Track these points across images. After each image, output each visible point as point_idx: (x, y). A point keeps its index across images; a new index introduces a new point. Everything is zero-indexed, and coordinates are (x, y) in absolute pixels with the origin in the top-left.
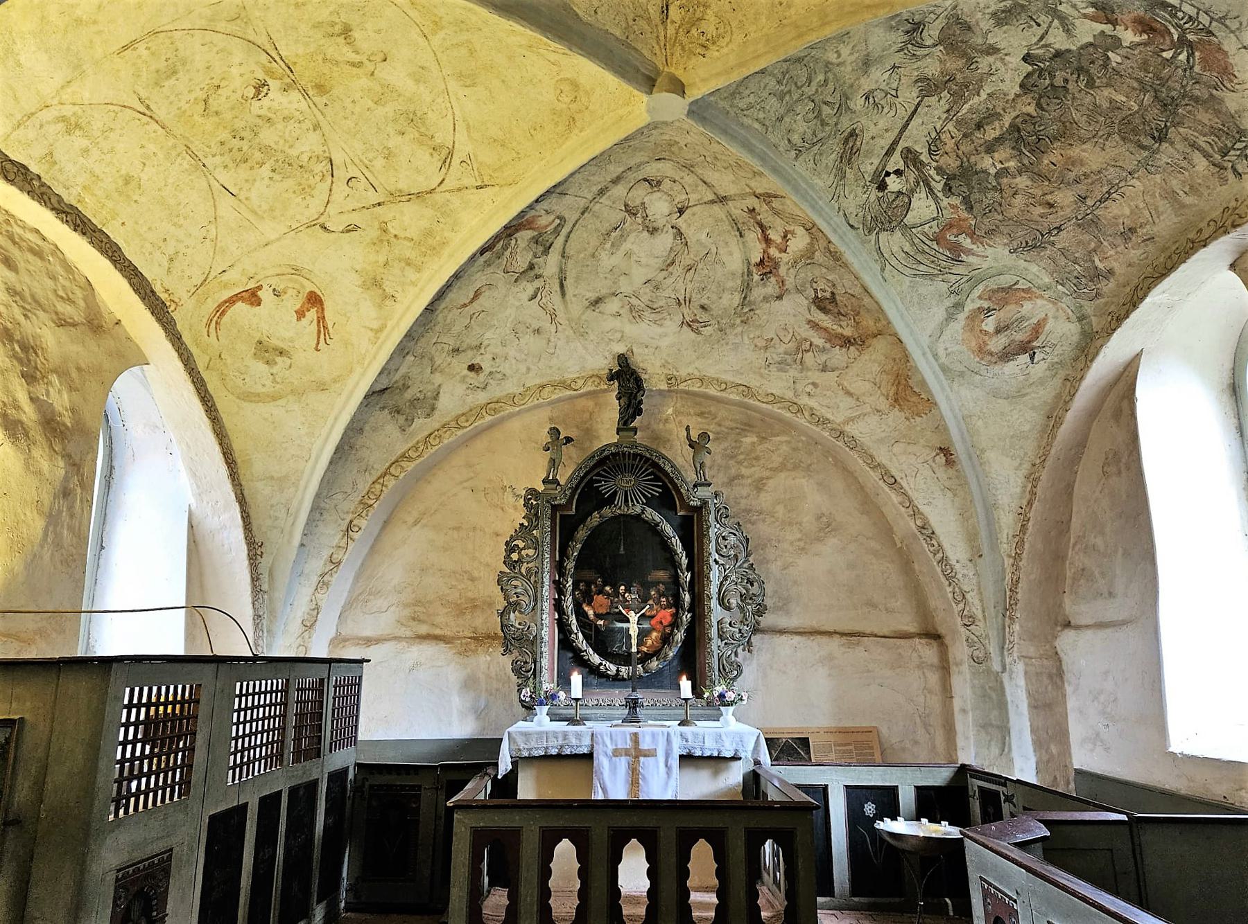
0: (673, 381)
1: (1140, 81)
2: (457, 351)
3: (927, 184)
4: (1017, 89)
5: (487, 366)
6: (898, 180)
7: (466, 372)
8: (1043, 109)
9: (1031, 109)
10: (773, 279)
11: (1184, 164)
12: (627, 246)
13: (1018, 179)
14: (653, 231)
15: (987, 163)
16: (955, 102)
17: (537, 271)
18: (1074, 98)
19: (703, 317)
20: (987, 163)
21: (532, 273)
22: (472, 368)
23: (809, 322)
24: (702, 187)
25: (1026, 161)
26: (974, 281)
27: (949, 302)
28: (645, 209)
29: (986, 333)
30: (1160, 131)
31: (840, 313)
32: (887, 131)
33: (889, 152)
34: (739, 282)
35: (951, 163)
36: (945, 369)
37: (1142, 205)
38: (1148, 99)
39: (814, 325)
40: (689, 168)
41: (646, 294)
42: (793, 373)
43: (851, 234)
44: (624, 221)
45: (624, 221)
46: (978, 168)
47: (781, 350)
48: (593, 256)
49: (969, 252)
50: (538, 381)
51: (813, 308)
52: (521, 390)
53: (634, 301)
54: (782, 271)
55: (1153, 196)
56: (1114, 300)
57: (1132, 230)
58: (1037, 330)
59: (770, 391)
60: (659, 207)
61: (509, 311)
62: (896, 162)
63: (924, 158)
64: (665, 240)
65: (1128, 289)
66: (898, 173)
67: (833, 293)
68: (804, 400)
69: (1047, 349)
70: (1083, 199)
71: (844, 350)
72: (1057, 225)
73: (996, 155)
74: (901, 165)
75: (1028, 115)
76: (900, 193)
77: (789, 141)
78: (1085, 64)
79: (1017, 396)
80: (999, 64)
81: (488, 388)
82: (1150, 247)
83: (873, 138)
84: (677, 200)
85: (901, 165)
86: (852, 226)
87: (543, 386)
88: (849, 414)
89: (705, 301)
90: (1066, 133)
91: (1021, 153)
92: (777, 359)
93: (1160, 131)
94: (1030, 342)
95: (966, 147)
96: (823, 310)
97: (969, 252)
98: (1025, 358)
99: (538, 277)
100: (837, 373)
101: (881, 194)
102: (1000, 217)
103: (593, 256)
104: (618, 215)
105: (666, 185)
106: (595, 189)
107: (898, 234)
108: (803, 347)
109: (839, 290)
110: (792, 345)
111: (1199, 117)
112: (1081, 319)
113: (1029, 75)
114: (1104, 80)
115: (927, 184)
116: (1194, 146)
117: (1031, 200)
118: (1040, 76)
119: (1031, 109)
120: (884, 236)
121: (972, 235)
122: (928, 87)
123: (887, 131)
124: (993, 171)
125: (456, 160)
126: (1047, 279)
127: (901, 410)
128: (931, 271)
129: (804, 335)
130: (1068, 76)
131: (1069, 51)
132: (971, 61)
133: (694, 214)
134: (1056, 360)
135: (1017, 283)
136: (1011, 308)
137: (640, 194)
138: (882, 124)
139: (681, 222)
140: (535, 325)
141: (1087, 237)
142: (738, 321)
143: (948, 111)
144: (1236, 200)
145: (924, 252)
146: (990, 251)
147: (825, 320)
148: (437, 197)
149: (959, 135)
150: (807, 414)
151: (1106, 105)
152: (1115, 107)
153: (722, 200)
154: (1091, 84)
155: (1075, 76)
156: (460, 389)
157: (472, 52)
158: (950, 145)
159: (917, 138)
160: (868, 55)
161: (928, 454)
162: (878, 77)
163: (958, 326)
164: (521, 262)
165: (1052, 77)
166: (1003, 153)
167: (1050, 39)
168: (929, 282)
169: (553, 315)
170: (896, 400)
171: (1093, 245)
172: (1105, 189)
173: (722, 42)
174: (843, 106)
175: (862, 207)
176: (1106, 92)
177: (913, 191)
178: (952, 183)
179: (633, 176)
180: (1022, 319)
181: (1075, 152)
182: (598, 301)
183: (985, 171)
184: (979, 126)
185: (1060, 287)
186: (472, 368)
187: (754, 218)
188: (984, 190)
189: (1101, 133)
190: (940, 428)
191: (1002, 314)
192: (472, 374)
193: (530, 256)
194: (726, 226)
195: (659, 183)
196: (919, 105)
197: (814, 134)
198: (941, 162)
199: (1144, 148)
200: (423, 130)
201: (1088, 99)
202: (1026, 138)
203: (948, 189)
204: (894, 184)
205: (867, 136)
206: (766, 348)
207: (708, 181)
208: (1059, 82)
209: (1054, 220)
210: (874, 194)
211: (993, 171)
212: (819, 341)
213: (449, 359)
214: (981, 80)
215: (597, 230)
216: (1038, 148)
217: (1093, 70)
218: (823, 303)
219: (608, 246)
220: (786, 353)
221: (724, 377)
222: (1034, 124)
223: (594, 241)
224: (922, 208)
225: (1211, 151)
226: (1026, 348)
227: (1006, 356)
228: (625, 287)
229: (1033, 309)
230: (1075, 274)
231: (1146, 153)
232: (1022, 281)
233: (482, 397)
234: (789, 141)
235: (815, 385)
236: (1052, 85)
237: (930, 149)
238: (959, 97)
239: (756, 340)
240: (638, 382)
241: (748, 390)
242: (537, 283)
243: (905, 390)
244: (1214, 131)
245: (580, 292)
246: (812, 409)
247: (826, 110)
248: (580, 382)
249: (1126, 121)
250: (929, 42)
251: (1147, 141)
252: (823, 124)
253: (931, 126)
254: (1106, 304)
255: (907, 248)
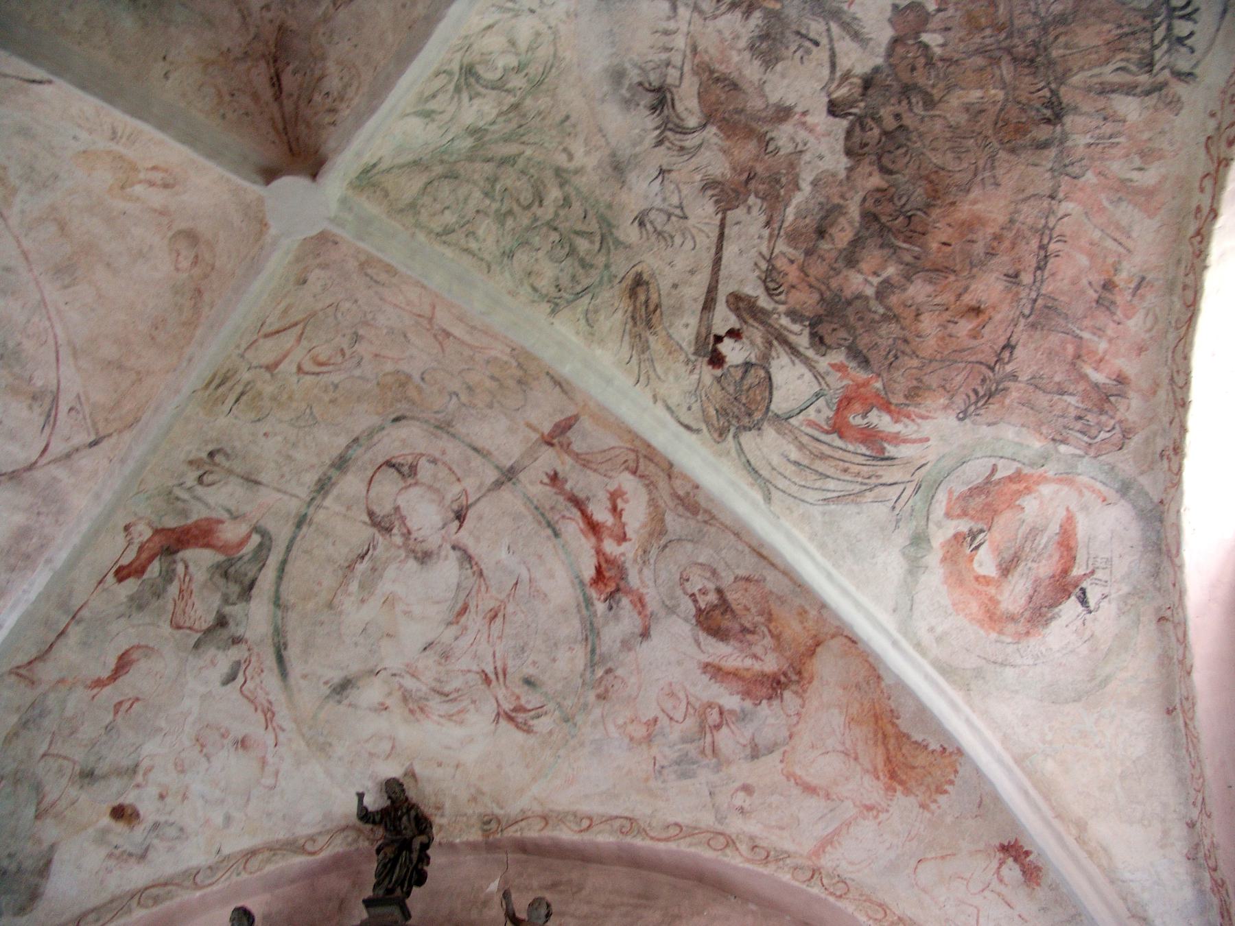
0: (494, 825)
1: (981, 51)
2: (88, 776)
3: (785, 342)
4: (845, 162)
5: (148, 808)
6: (738, 346)
7: (106, 820)
8: (891, 172)
9: (876, 180)
10: (625, 601)
11: (1108, 128)
12: (386, 586)
13: (912, 290)
14: (425, 557)
15: (859, 282)
16: (772, 208)
17: (233, 629)
18: (920, 135)
19: (531, 699)
20: (859, 282)
21: (225, 634)
22: (119, 813)
23: (706, 667)
24: (477, 461)
25: (908, 258)
26: (927, 489)
27: (901, 538)
28: (403, 519)
29: (987, 581)
30: (1049, 104)
31: (744, 630)
32: (692, 272)
33: (709, 304)
34: (576, 623)
35: (806, 299)
36: (946, 670)
37: (1097, 235)
38: (1006, 70)
39: (716, 671)
40: (444, 427)
41: (429, 666)
42: (705, 776)
43: (692, 438)
44: (372, 545)
45: (372, 545)
46: (848, 293)
47: (675, 736)
48: (330, 605)
49: (897, 439)
50: (247, 843)
51: (702, 636)
52: (212, 859)
53: (409, 683)
54: (634, 580)
55: (1102, 209)
56: (1154, 427)
57: (1108, 286)
58: (1067, 543)
59: (671, 820)
60: (424, 515)
61: (187, 703)
62: (723, 319)
63: (764, 302)
64: (447, 571)
65: (1162, 394)
66: (734, 334)
67: (719, 591)
68: (736, 825)
69: (1099, 574)
70: (1013, 277)
71: (776, 703)
72: (1002, 341)
73: (863, 266)
74: (733, 322)
75: (878, 190)
76: (747, 365)
77: (535, 289)
78: (905, 77)
79: (1090, 690)
80: (802, 134)
81: (151, 855)
82: (1151, 297)
83: (675, 286)
84: (449, 497)
85: (733, 322)
86: (688, 427)
87: (253, 853)
88: (821, 830)
89: (530, 671)
90: (938, 191)
91: (896, 249)
92: (673, 755)
93: (1049, 104)
94: (1065, 572)
95: (817, 269)
96: (718, 633)
97: (897, 439)
98: (1071, 607)
99: (236, 641)
100: (777, 755)
101: (718, 372)
102: (915, 362)
103: (330, 605)
104: (359, 533)
105: (425, 471)
106: (311, 478)
107: (770, 432)
108: (711, 721)
109: (727, 579)
110: (691, 723)
111: (1083, 43)
112: (1125, 489)
113: (849, 133)
114: (941, 85)
115: (785, 342)
116: (1106, 90)
117: (946, 316)
118: (863, 128)
119: (876, 180)
120: (747, 438)
121: (886, 407)
122: (727, 195)
123: (692, 272)
124: (870, 291)
125: (63, 407)
126: (1037, 444)
127: (908, 792)
128: (850, 487)
129: (706, 696)
130: (898, 109)
131: (876, 70)
132: (765, 142)
133: (480, 518)
134: (1125, 589)
135: (994, 470)
136: (1005, 520)
137: (387, 490)
138: (682, 263)
139: (465, 537)
140: (238, 730)
141: (1054, 339)
142: (591, 697)
143: (768, 224)
144: (1213, 115)
145: (823, 457)
146: (927, 428)
147: (727, 654)
148: (39, 475)
149: (799, 256)
150: (743, 848)
151: (963, 118)
152: (974, 111)
153: (509, 475)
154: (930, 103)
155: (904, 103)
156: (95, 858)
157: (62, 227)
158: (793, 274)
159: (742, 274)
160: (613, 155)
161: (982, 868)
162: (641, 191)
163: (934, 577)
164: (202, 611)
165: (878, 120)
166: (871, 257)
167: (844, 63)
168: (852, 509)
169: (269, 714)
170: (893, 775)
171: (1070, 349)
172: (1034, 244)
173: (350, 92)
174: (607, 238)
175: (695, 391)
176: (954, 100)
177: (766, 357)
178: (824, 329)
179: (367, 457)
180: (1034, 532)
181: (964, 210)
182: (343, 687)
183: (859, 297)
184: (821, 233)
185: (1063, 448)
186: (119, 813)
187: (562, 491)
188: (872, 326)
189: (981, 163)
190: (987, 802)
191: (997, 534)
192: (120, 827)
193: (216, 601)
194: (529, 524)
195: (413, 469)
196: (722, 226)
197: (573, 277)
198: (792, 301)
199: (1044, 145)
200: (17, 370)
201: (938, 125)
202: (892, 223)
203: (818, 341)
204: (733, 352)
205: (665, 284)
206: (649, 739)
207: (479, 444)
208: (890, 123)
209: (994, 335)
210: (708, 374)
211: (870, 291)
212: (732, 701)
213: (73, 792)
214: (792, 166)
215: (330, 560)
216: (913, 230)
217: (920, 78)
218: (715, 619)
219: (354, 587)
220: (684, 740)
221: (585, 808)
222: (891, 200)
223: (329, 580)
224: (792, 382)
225: (1127, 78)
226: (1065, 586)
227: (1039, 613)
228: (393, 662)
229: (1044, 506)
230: (1073, 413)
231: (1053, 152)
232: (1000, 463)
233: (138, 876)
234: (535, 289)
235: (747, 789)
236: (885, 133)
237: (767, 289)
238: (774, 199)
239: (630, 728)
240: (423, 824)
241: (631, 824)
242: (235, 653)
243: (906, 752)
244: (1116, 46)
245: (315, 667)
246: (752, 838)
247: (583, 245)
248: (322, 841)
249: (1001, 123)
250: (692, 122)
251: (1043, 133)
252: (584, 264)
253: (753, 252)
254: (1147, 441)
255: (794, 454)
